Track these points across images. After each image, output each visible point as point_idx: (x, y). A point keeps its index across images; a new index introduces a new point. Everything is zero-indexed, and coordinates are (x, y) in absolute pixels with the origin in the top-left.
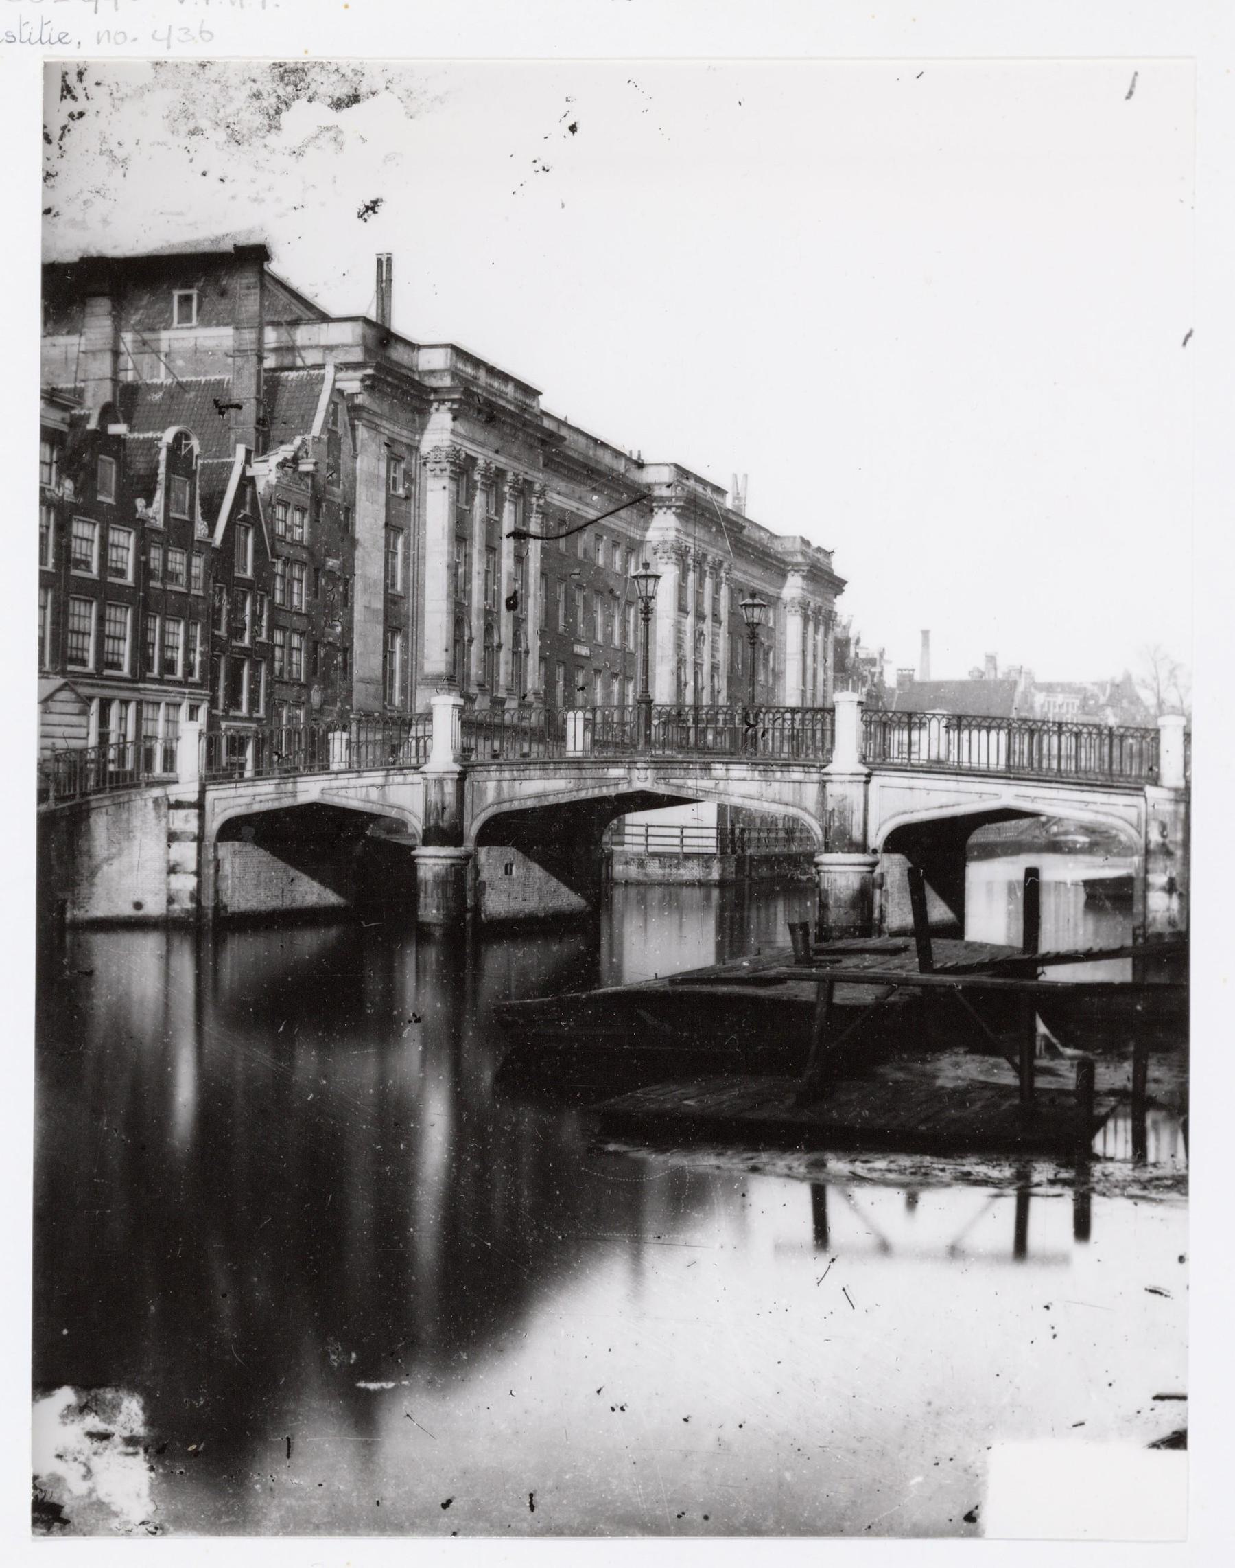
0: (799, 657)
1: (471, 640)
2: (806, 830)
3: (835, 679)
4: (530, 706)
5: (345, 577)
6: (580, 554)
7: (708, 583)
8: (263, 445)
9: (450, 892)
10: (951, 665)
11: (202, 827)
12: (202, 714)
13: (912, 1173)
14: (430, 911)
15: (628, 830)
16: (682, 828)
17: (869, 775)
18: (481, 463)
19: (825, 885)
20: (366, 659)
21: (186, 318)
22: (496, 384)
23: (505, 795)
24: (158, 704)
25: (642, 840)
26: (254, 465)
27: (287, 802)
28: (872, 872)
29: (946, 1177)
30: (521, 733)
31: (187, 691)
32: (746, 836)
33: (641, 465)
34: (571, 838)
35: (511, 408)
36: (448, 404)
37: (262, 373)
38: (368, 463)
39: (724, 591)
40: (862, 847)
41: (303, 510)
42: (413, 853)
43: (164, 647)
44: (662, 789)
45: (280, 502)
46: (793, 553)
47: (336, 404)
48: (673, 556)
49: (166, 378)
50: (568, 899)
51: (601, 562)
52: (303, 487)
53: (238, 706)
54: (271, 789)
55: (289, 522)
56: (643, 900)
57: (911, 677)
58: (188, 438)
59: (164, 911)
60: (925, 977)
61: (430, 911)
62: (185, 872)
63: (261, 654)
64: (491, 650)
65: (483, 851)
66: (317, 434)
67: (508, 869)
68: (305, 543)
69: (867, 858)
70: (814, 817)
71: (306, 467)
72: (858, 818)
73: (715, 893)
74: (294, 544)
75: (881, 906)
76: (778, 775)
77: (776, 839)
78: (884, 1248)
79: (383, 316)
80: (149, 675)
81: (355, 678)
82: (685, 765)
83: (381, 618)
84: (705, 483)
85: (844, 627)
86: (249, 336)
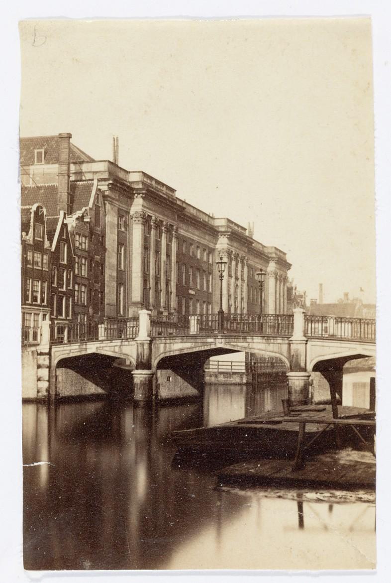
0: (274, 295)
1: (150, 288)
2: (281, 361)
3: (287, 303)
4: (172, 314)
5: (102, 264)
6: (191, 254)
7: (240, 265)
8: (70, 211)
9: (146, 388)
10: (331, 297)
11: (50, 363)
12: (48, 317)
13: (340, 498)
14: (139, 395)
15: (211, 363)
16: (232, 362)
17: (307, 341)
18: (153, 218)
19: (290, 384)
20: (110, 296)
21: (39, 160)
22: (149, 181)
23: (168, 349)
24: (31, 314)
25: (230, 367)
26: (67, 219)
27: (83, 353)
28: (308, 379)
29: (353, 499)
30: (174, 325)
31: (41, 308)
32: (256, 365)
33: (213, 218)
34: (190, 366)
35: (165, 196)
36: (141, 195)
37: (70, 183)
38: (111, 218)
39: (246, 269)
40: (305, 370)
41: (86, 237)
42: (132, 372)
43: (33, 291)
44: (228, 347)
45: (77, 233)
46: (271, 253)
47: (98, 195)
48: (227, 254)
49: (33, 184)
50: (191, 391)
51: (199, 257)
52: (86, 227)
53: (61, 314)
54: (77, 347)
55: (80, 242)
56: (216, 391)
57: (316, 303)
58: (42, 208)
59: (36, 396)
60: (335, 420)
61: (139, 395)
62: (44, 381)
63: (70, 294)
64: (157, 291)
65: (159, 372)
66: (91, 207)
67: (168, 379)
68: (86, 250)
69: (306, 374)
70: (286, 358)
71: (87, 220)
72: (303, 358)
73: (245, 388)
74: (82, 250)
75: (312, 393)
76: (272, 341)
77: (267, 366)
78: (326, 528)
79: (115, 161)
80: (27, 302)
81: (106, 304)
82: (237, 337)
83: (116, 279)
84: (238, 226)
85: (290, 283)
86: (65, 168)
